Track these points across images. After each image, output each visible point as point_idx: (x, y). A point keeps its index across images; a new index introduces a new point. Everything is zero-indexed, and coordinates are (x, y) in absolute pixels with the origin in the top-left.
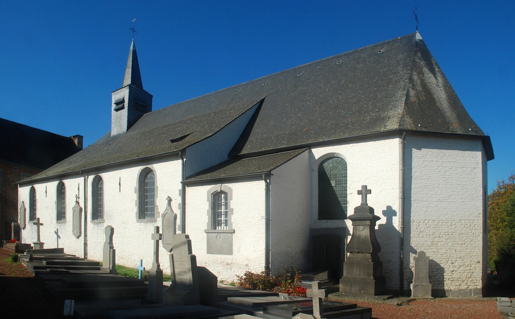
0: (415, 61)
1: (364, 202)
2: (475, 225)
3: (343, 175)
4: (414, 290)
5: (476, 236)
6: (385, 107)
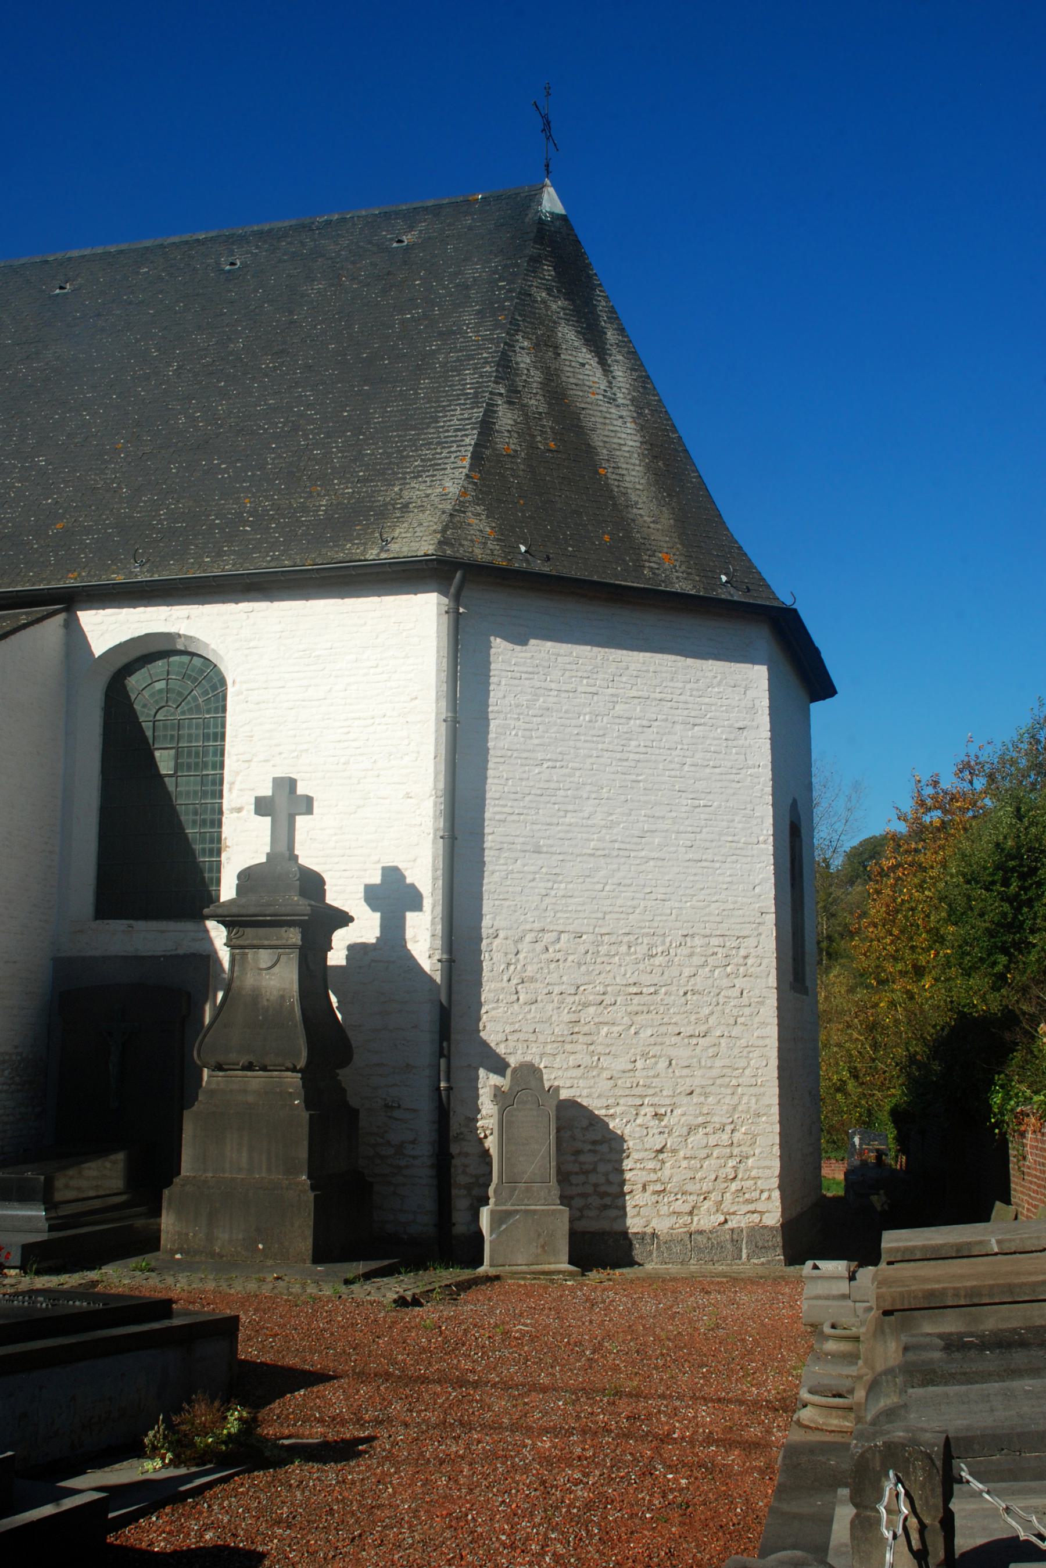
0: (530, 295)
1: (283, 848)
2: (746, 957)
3: (209, 728)
4: (494, 1236)
5: (753, 1005)
6: (394, 463)
